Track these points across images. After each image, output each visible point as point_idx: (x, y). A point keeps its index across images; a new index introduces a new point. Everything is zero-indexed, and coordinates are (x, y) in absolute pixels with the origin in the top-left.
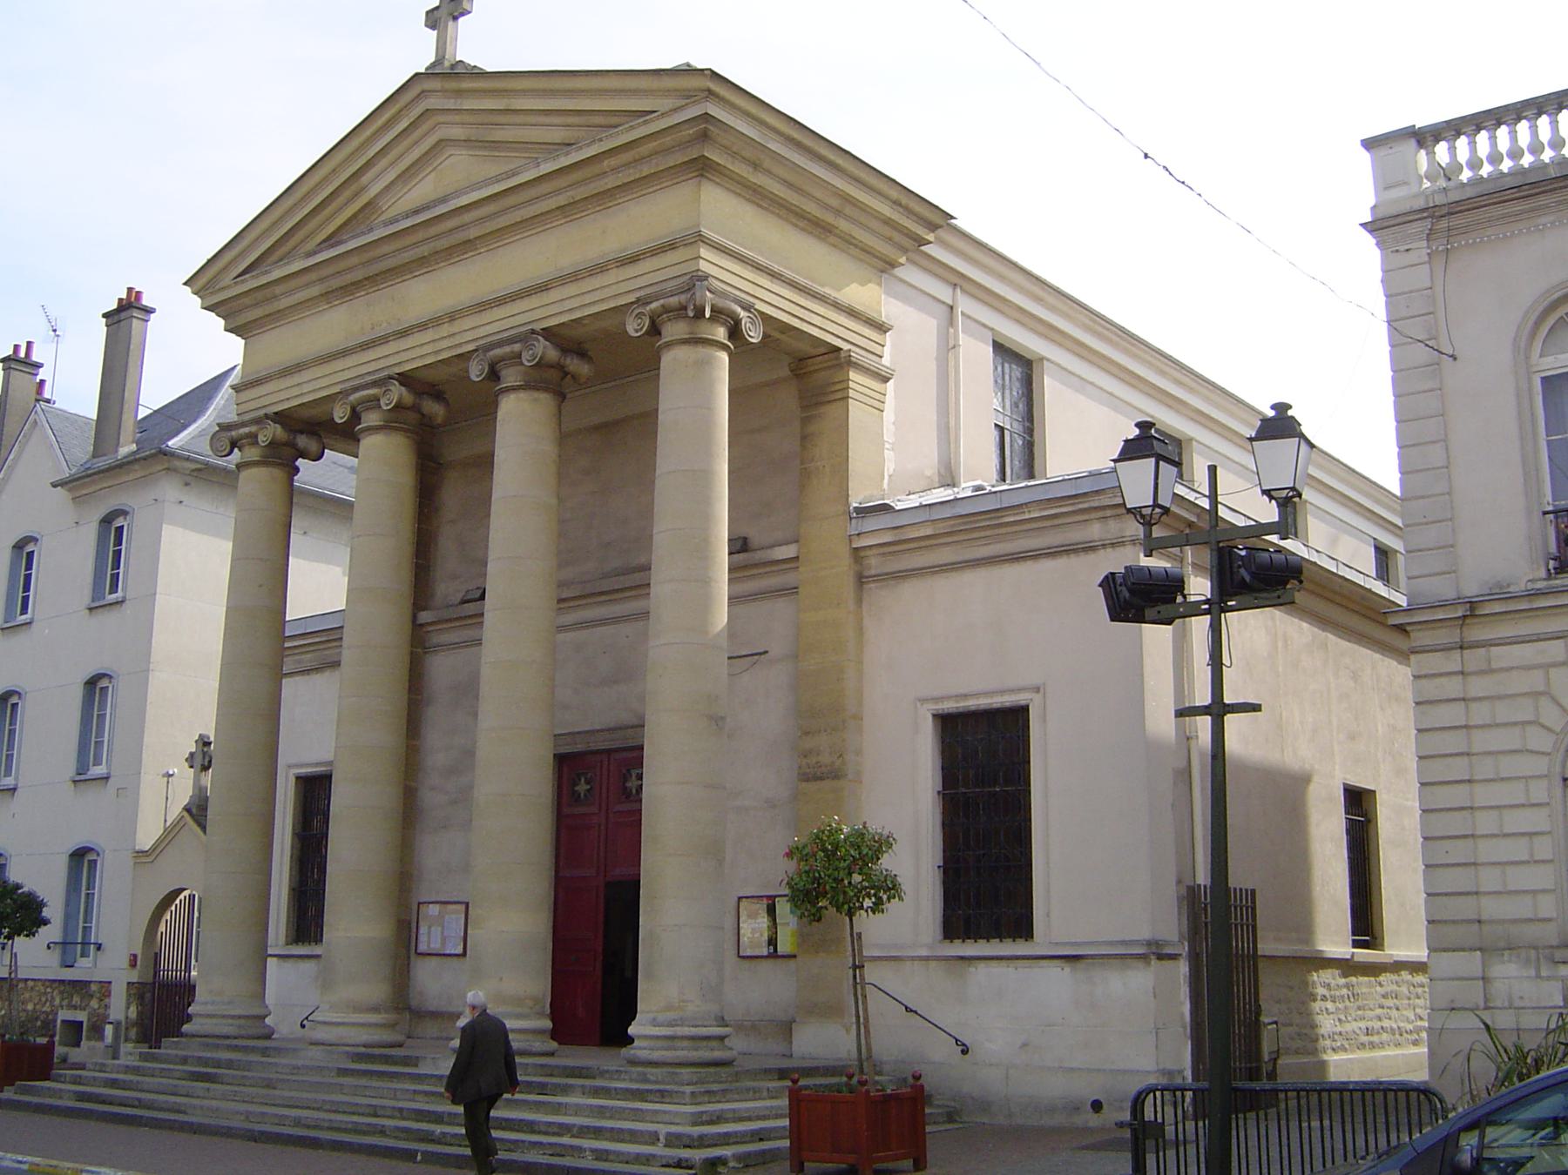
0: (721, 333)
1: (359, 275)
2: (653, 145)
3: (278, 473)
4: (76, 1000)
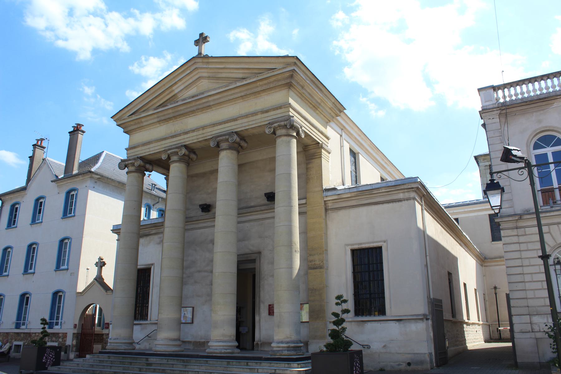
0: (295, 134)
1: (171, 116)
2: (274, 78)
3: (140, 175)
4: (54, 339)
